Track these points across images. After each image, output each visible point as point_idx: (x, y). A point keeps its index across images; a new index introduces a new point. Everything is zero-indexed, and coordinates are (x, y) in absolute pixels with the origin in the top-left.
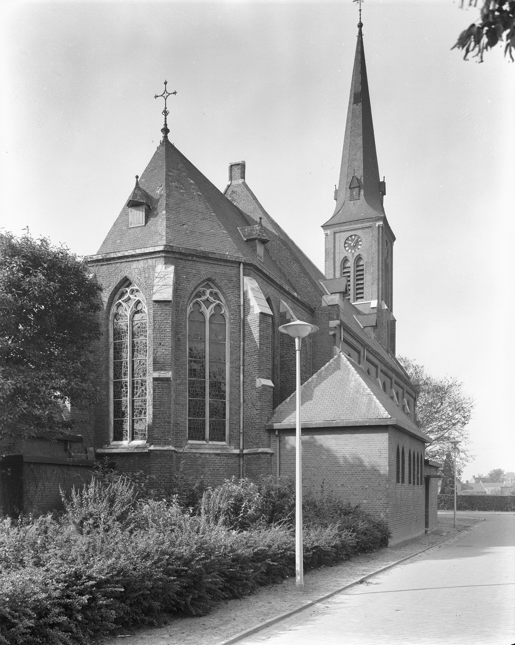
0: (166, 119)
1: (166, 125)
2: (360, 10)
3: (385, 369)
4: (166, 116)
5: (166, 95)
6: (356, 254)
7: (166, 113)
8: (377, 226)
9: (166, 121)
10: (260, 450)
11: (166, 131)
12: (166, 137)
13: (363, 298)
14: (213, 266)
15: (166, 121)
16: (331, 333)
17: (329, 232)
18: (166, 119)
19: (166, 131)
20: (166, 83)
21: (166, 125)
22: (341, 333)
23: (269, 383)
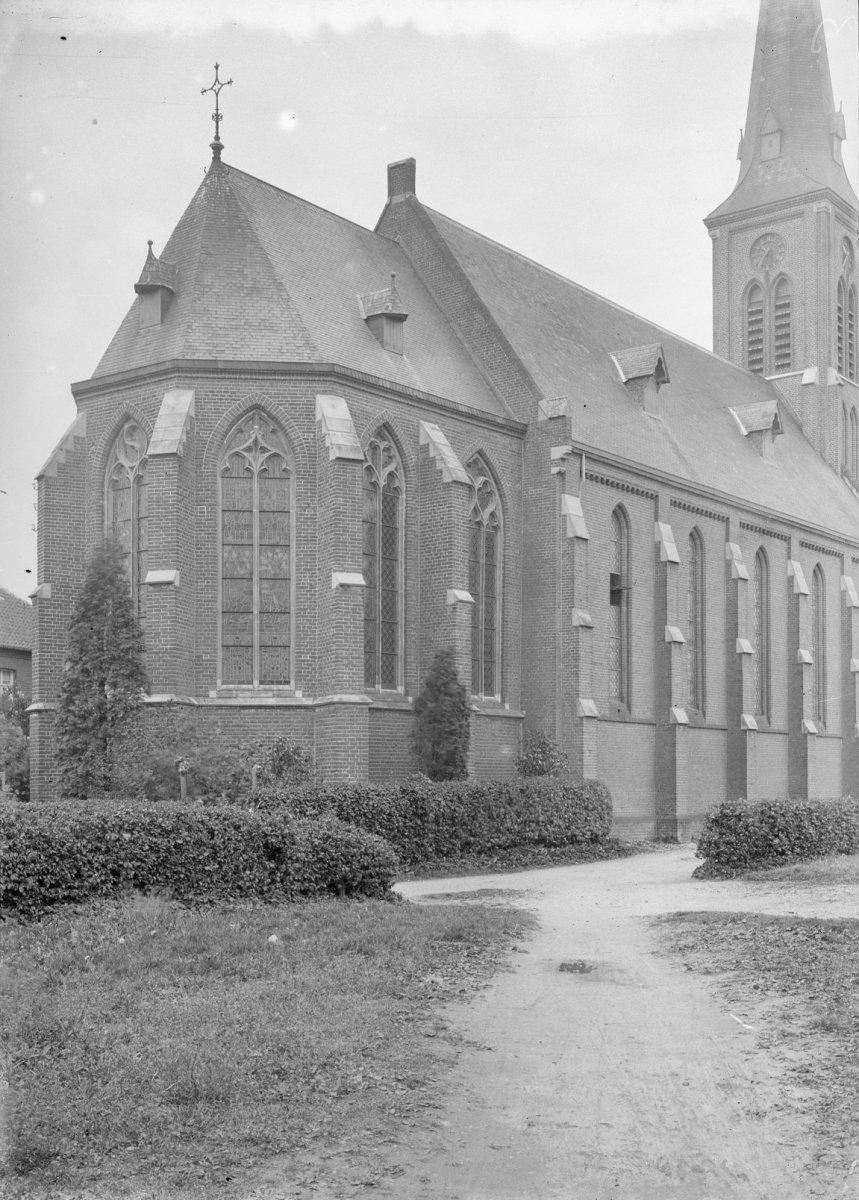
0: (217, 128)
1: (217, 138)
2: (217, 118)
3: (747, 519)
4: (217, 123)
5: (217, 86)
6: (773, 274)
7: (217, 118)
8: (815, 210)
9: (217, 132)
10: (336, 698)
11: (217, 148)
12: (217, 158)
13: (788, 365)
14: (263, 383)
15: (217, 132)
16: (555, 470)
17: (718, 232)
18: (217, 128)
19: (217, 148)
20: (217, 67)
21: (217, 138)
22: (581, 463)
23: (358, 579)
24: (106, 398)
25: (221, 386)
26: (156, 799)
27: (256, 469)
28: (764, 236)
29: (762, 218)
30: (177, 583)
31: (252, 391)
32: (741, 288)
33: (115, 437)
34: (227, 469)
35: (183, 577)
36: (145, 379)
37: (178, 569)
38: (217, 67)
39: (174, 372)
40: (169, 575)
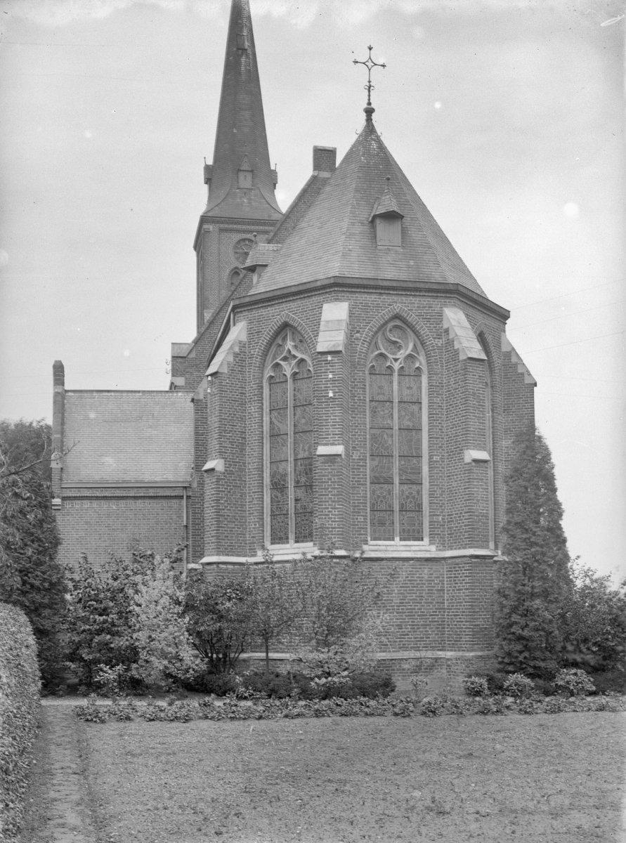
0: (369, 96)
1: (369, 104)
4: (369, 91)
9: (369, 100)
15: (369, 100)
18: (369, 96)
21: (369, 104)
24: (373, 297)
25: (371, 298)
26: (281, 698)
27: (288, 372)
28: (244, 240)
29: (239, 227)
30: (343, 457)
31: (400, 304)
32: (228, 271)
33: (281, 330)
34: (271, 377)
35: (346, 449)
36: (420, 291)
37: (343, 444)
38: (383, 66)
39: (454, 293)
40: (339, 449)
